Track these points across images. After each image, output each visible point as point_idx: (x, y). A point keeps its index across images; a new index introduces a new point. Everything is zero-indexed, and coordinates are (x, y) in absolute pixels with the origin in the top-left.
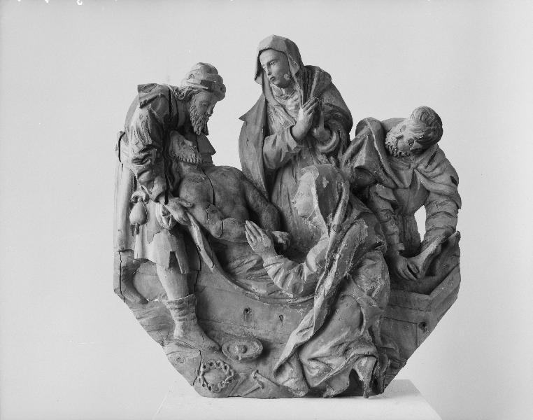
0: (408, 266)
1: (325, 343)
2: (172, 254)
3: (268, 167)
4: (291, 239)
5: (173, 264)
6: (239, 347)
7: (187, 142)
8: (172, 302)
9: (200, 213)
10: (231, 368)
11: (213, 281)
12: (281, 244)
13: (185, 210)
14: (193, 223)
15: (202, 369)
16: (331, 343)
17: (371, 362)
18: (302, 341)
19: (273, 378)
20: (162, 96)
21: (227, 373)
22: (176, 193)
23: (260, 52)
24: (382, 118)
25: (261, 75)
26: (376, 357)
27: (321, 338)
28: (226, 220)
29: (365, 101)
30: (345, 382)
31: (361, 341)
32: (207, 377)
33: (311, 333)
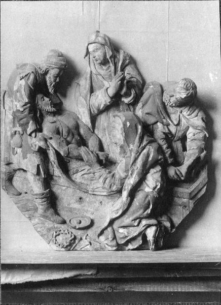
0: (6, 92)
1: (129, 217)
2: (38, 166)
3: (93, 112)
4: (107, 158)
5: (38, 173)
6: (76, 221)
7: (45, 98)
8: (36, 195)
9: (53, 143)
10: (72, 233)
11: (61, 185)
12: (102, 160)
13: (46, 140)
14: (51, 148)
15: (55, 234)
16: (131, 218)
17: (154, 229)
18: (114, 217)
19: (97, 240)
20: (33, 72)
21: (70, 236)
22: (41, 130)
23: (88, 45)
24: (162, 81)
25: (88, 56)
26: (153, 225)
27: (126, 216)
28: (69, 145)
29: (154, 72)
30: (139, 242)
31: (149, 217)
32: (57, 238)
33: (120, 212)
